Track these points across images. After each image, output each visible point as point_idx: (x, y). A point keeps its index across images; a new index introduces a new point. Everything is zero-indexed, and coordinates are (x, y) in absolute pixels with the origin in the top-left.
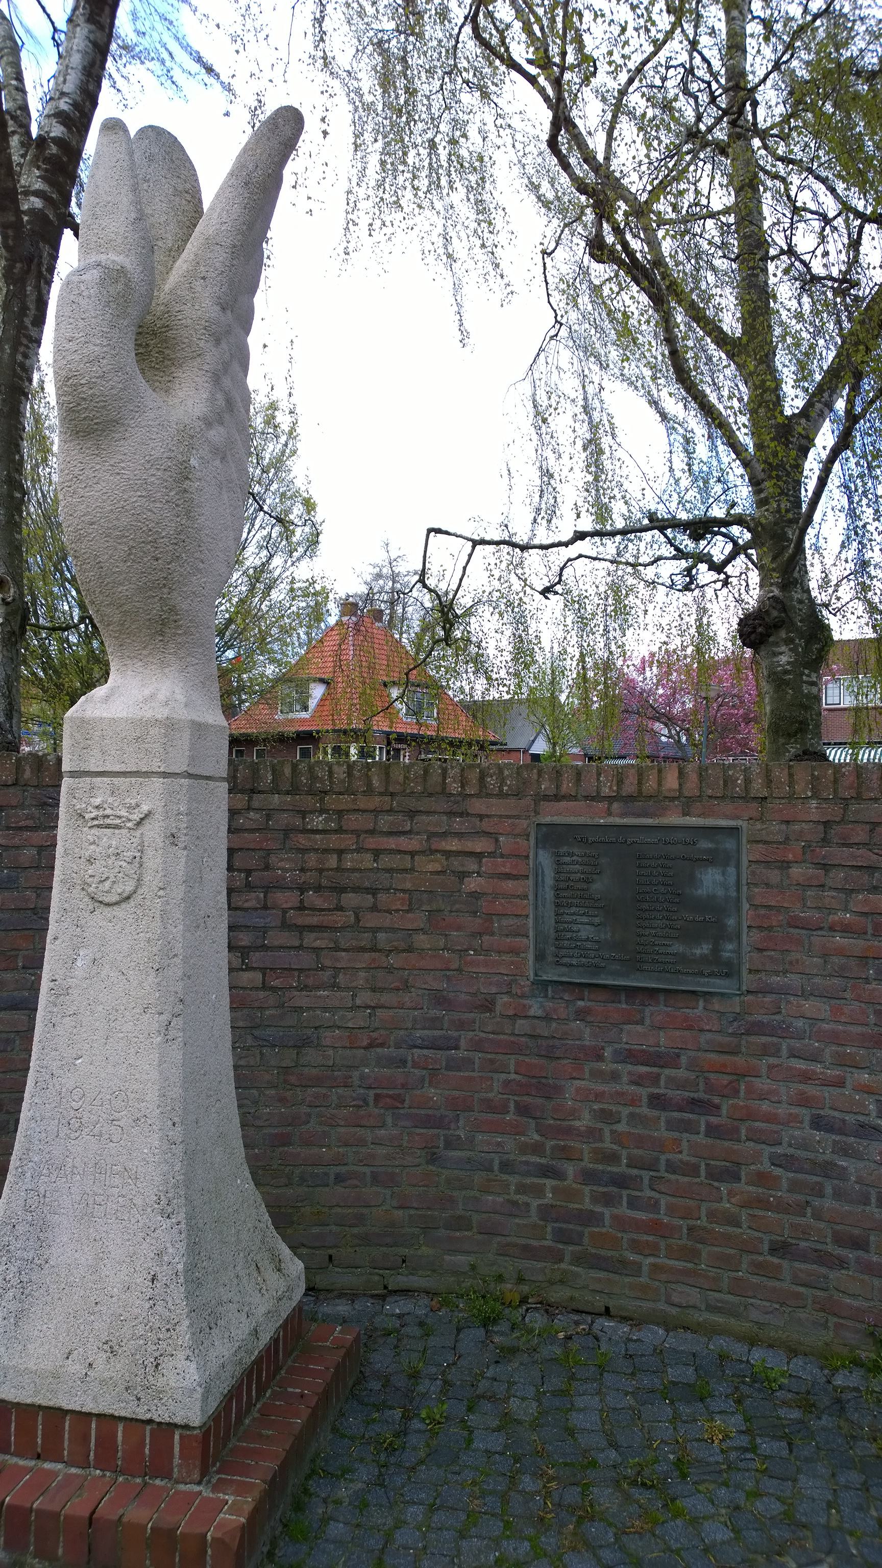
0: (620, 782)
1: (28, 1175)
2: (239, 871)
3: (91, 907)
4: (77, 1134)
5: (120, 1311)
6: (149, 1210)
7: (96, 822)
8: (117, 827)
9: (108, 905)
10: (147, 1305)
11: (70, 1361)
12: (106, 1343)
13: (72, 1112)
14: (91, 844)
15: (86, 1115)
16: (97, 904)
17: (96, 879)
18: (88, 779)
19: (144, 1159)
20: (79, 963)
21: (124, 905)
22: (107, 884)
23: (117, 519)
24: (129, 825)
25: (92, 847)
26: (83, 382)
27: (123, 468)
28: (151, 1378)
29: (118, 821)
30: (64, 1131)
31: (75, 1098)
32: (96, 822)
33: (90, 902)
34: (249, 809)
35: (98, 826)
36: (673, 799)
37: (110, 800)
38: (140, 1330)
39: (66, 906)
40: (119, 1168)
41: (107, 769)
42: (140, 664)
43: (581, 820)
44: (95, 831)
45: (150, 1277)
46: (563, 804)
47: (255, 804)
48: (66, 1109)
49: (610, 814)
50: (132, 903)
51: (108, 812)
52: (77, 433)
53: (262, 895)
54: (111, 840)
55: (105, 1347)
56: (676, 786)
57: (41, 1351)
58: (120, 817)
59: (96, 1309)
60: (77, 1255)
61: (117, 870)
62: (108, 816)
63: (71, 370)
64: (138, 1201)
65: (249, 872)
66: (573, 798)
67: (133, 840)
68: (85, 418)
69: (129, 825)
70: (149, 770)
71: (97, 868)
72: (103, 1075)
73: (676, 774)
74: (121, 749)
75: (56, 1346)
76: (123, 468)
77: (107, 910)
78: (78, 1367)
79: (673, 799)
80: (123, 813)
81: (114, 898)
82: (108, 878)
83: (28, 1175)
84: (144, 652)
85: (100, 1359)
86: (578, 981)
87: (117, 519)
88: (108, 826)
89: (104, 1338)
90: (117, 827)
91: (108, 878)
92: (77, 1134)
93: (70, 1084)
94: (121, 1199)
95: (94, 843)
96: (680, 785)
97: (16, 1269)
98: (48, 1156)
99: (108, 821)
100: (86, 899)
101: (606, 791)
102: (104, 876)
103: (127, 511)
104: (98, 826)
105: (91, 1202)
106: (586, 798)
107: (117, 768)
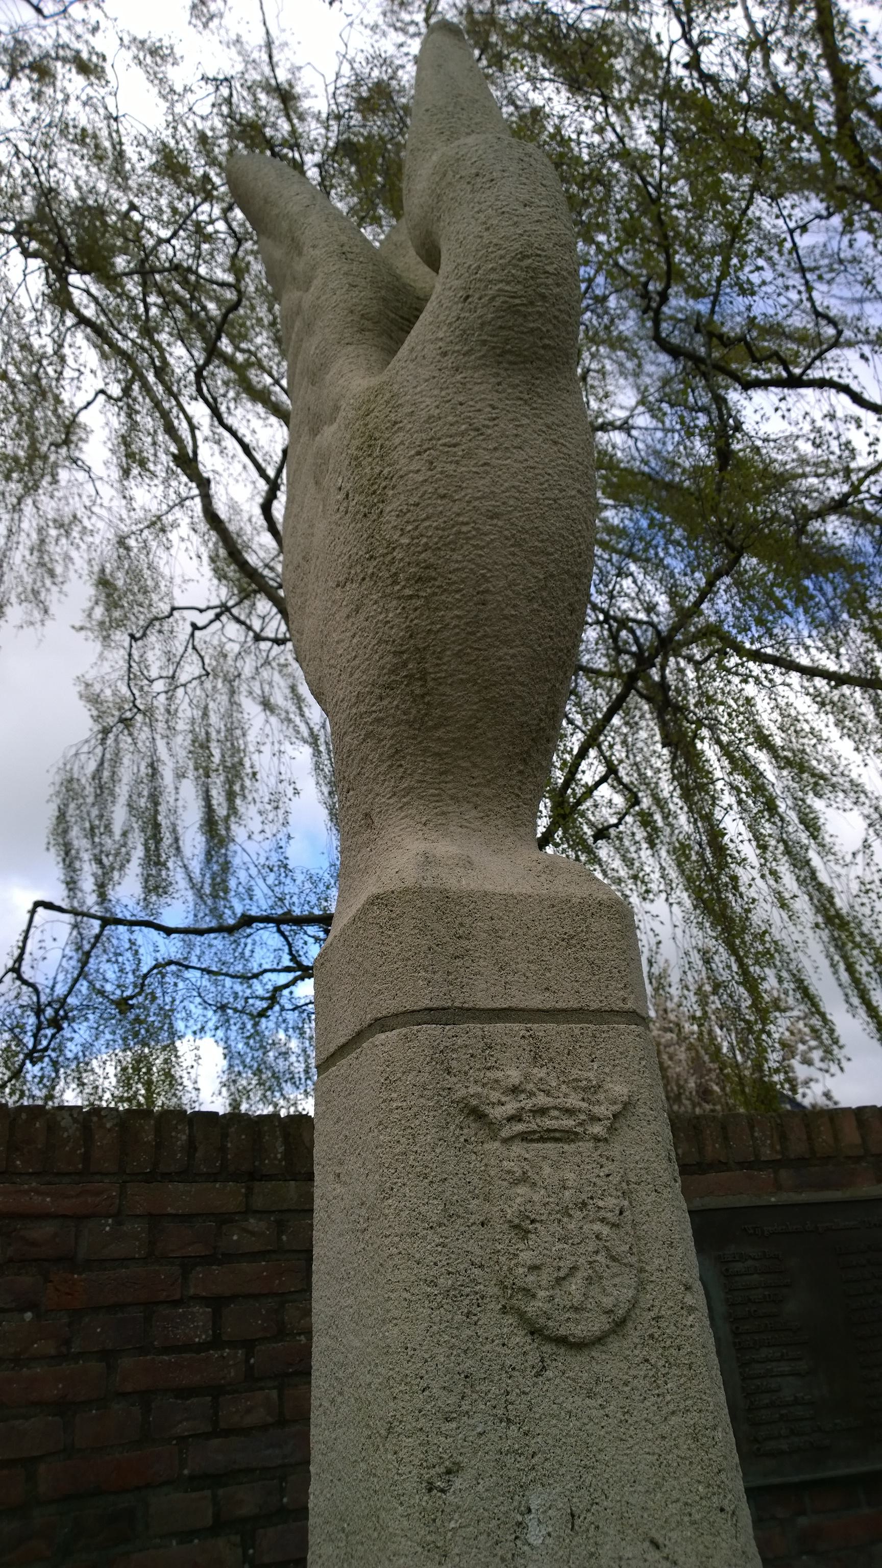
0: (783, 1138)
2: (232, 1344)
3: (533, 1359)
7: (519, 1127)
8: (569, 1136)
9: (579, 1346)
14: (516, 1182)
16: (548, 1348)
17: (546, 1277)
18: (475, 1028)
20: (535, 1535)
21: (614, 1345)
22: (575, 1286)
23: (543, 517)
24: (597, 1129)
25: (521, 1190)
26: (549, 268)
27: (564, 436)
29: (568, 1123)
32: (519, 1127)
33: (531, 1346)
34: (248, 1211)
35: (525, 1137)
36: (858, 1159)
37: (539, 1073)
39: (468, 1364)
41: (514, 1003)
42: (474, 813)
43: (744, 1200)
44: (517, 1149)
46: (712, 1176)
47: (258, 1202)
49: (778, 1187)
50: (634, 1336)
51: (542, 1100)
52: (504, 353)
53: (274, 1394)
54: (562, 1170)
56: (858, 1140)
58: (570, 1112)
61: (592, 1246)
62: (542, 1111)
63: (531, 245)
65: (249, 1345)
66: (720, 1166)
67: (609, 1167)
68: (532, 330)
69: (597, 1129)
70: (604, 1005)
71: (545, 1244)
73: (854, 1123)
74: (539, 960)
76: (564, 436)
77: (575, 1362)
79: (858, 1159)
80: (574, 1101)
81: (596, 1324)
82: (574, 1269)
84: (486, 791)
86: (796, 1479)
87: (543, 517)
88: (547, 1136)
90: (569, 1136)
91: (574, 1269)
95: (524, 1179)
96: (863, 1138)
99: (548, 1123)
100: (520, 1338)
101: (767, 1153)
102: (566, 1264)
103: (560, 508)
104: (525, 1137)
106: (742, 1165)
107: (536, 1001)
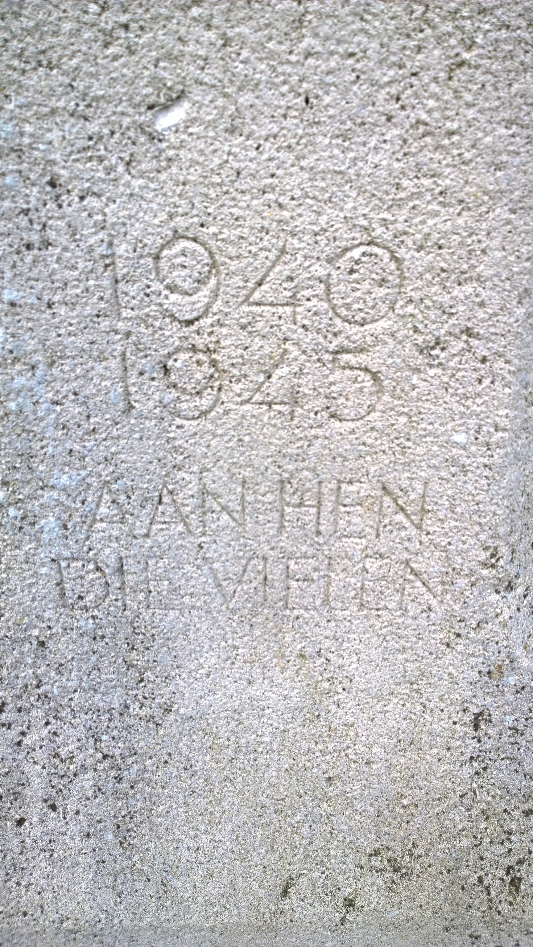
1: (50, 522)
4: (205, 402)
5: (399, 787)
6: (462, 582)
10: (468, 771)
11: (293, 900)
12: (377, 853)
13: (174, 334)
15: (230, 342)
19: (454, 461)
28: (505, 908)
30: (151, 395)
31: (177, 276)
38: (458, 818)
40: (364, 489)
45: (468, 718)
48: (144, 320)
55: (376, 862)
57: (213, 889)
59: (332, 791)
60: (252, 691)
64: (431, 564)
72: (294, 181)
75: (247, 876)
78: (319, 909)
83: (50, 522)
85: (372, 890)
89: (369, 843)
92: (205, 402)
93: (149, 221)
94: (372, 565)
97: (81, 732)
98: (106, 472)
105: (276, 573)
